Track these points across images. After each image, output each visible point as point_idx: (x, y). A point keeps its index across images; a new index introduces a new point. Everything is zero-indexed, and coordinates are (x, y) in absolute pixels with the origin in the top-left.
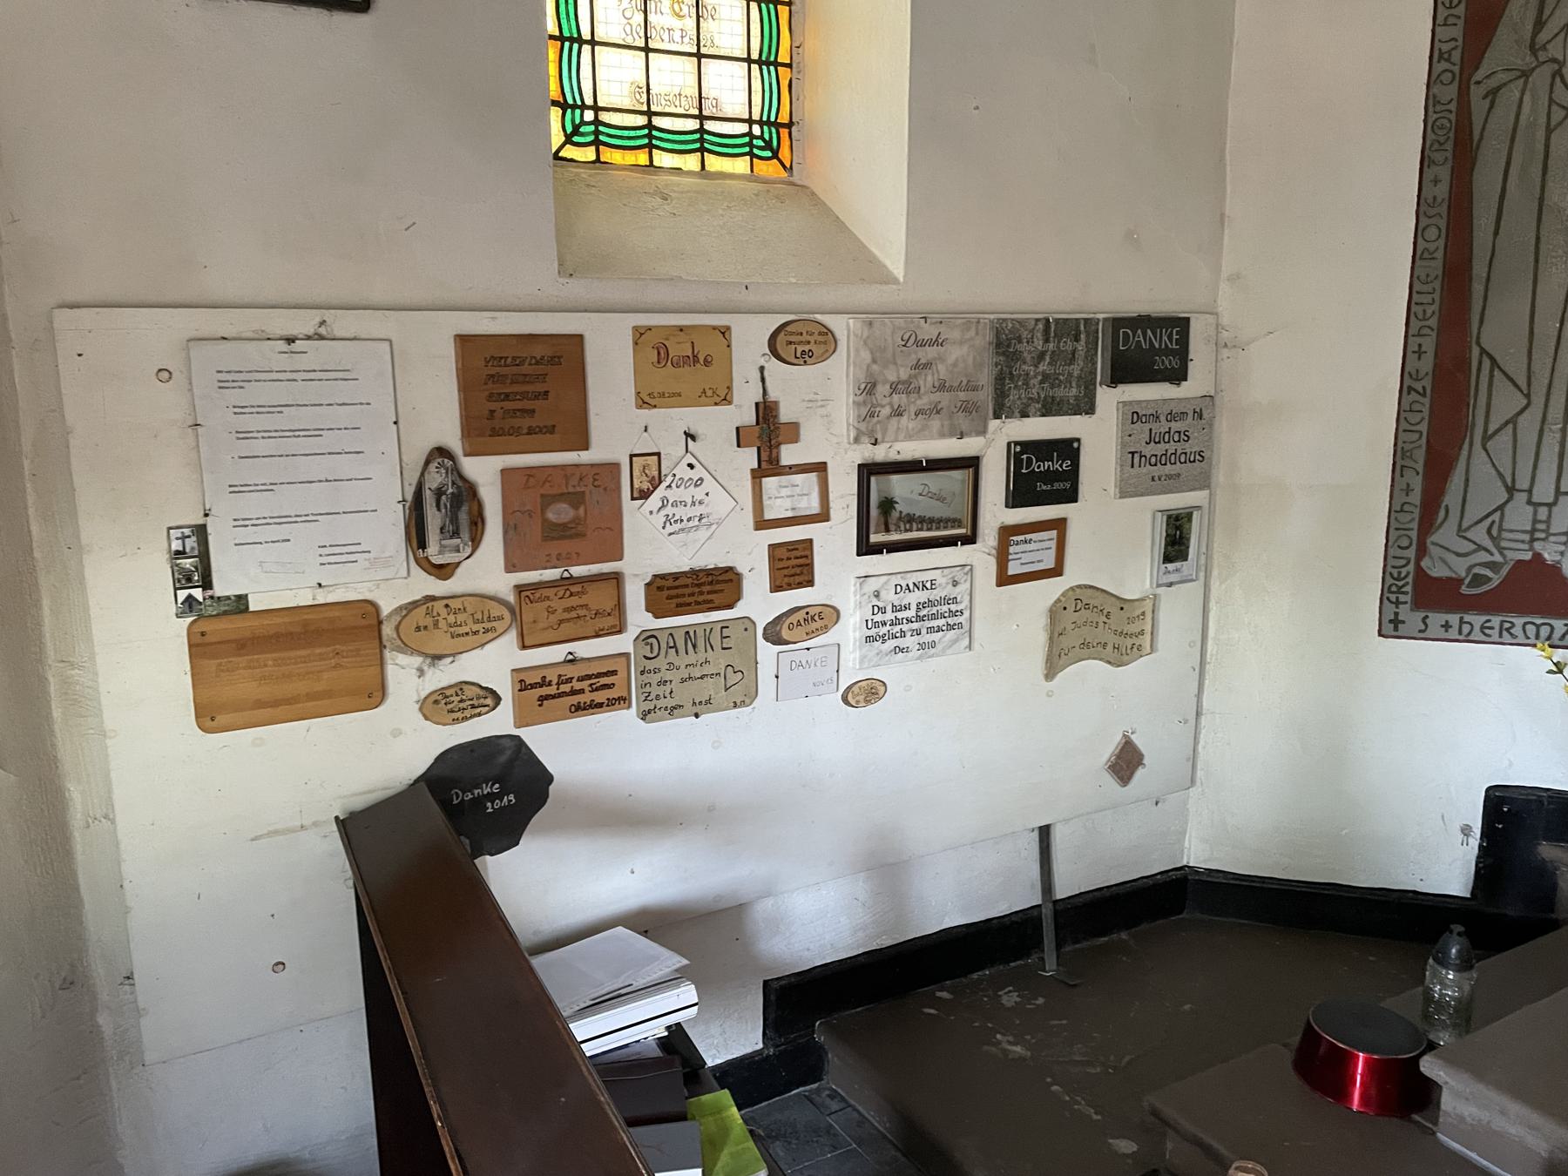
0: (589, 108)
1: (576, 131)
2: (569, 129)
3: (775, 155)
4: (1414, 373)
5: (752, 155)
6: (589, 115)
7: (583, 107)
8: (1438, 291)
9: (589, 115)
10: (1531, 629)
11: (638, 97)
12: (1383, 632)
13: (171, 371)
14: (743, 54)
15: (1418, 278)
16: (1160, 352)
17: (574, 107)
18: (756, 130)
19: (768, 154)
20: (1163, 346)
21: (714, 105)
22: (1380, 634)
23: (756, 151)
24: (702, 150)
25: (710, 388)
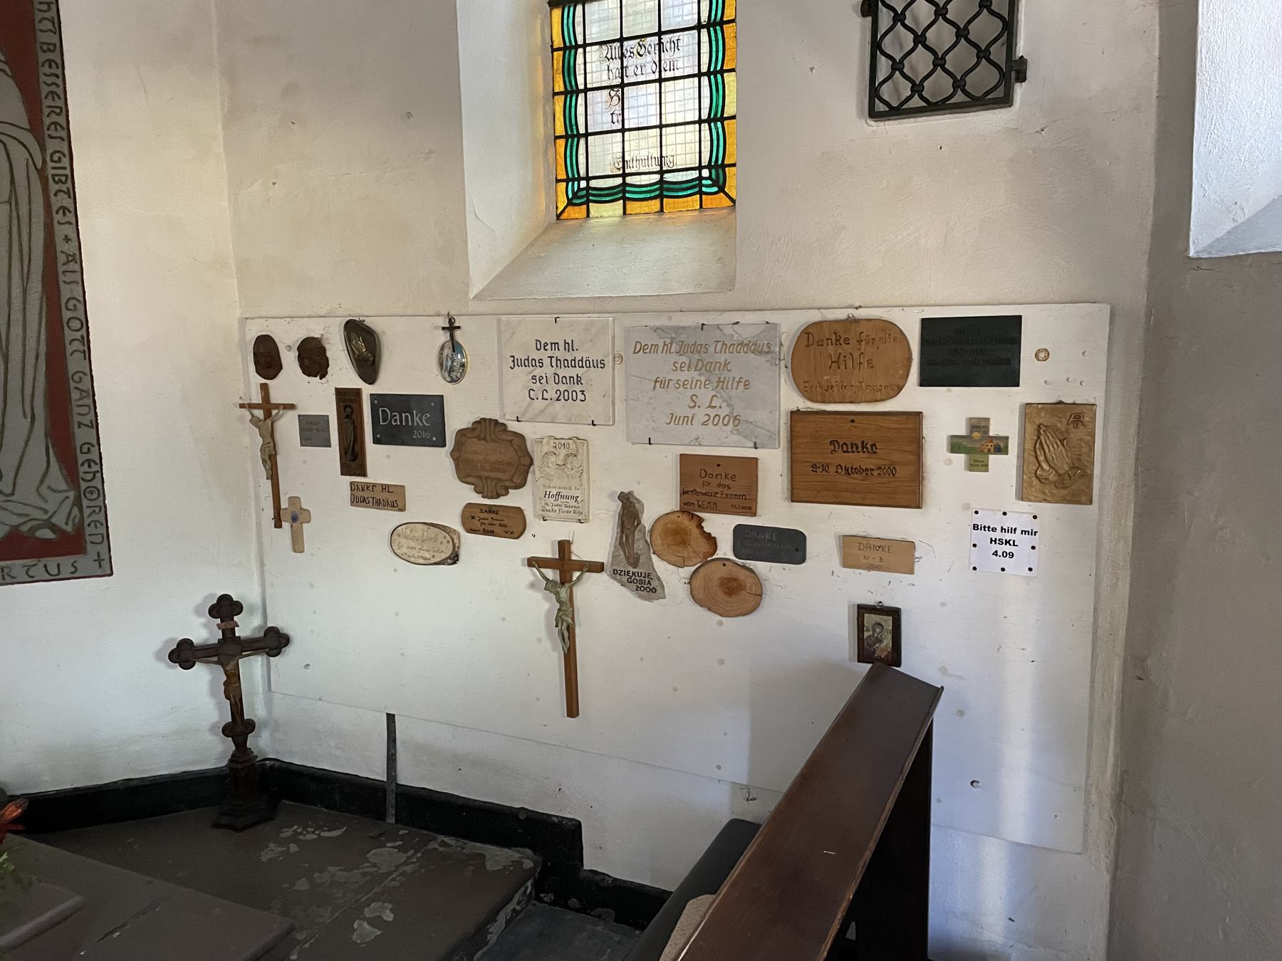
0: (583, 179)
1: (575, 194)
2: (570, 196)
3: (722, 190)
4: (98, 525)
5: (701, 193)
6: (583, 184)
7: (580, 179)
8: (67, 342)
9: (705, 173)
10: (69, 277)
11: (616, 165)
12: (109, 572)
13: (61, 226)
14: (591, 129)
15: (102, 524)
16: (418, 427)
17: (573, 180)
18: (705, 173)
19: (715, 189)
20: (415, 424)
21: (671, 161)
22: (111, 574)
23: (704, 189)
24: (661, 197)
25: (547, 350)
